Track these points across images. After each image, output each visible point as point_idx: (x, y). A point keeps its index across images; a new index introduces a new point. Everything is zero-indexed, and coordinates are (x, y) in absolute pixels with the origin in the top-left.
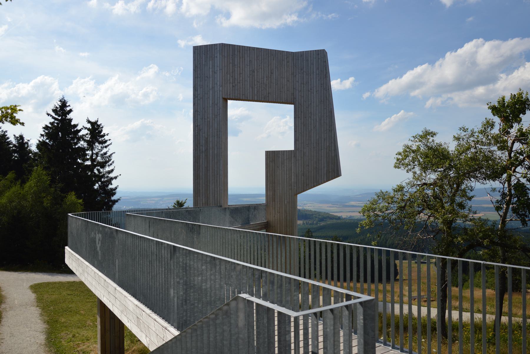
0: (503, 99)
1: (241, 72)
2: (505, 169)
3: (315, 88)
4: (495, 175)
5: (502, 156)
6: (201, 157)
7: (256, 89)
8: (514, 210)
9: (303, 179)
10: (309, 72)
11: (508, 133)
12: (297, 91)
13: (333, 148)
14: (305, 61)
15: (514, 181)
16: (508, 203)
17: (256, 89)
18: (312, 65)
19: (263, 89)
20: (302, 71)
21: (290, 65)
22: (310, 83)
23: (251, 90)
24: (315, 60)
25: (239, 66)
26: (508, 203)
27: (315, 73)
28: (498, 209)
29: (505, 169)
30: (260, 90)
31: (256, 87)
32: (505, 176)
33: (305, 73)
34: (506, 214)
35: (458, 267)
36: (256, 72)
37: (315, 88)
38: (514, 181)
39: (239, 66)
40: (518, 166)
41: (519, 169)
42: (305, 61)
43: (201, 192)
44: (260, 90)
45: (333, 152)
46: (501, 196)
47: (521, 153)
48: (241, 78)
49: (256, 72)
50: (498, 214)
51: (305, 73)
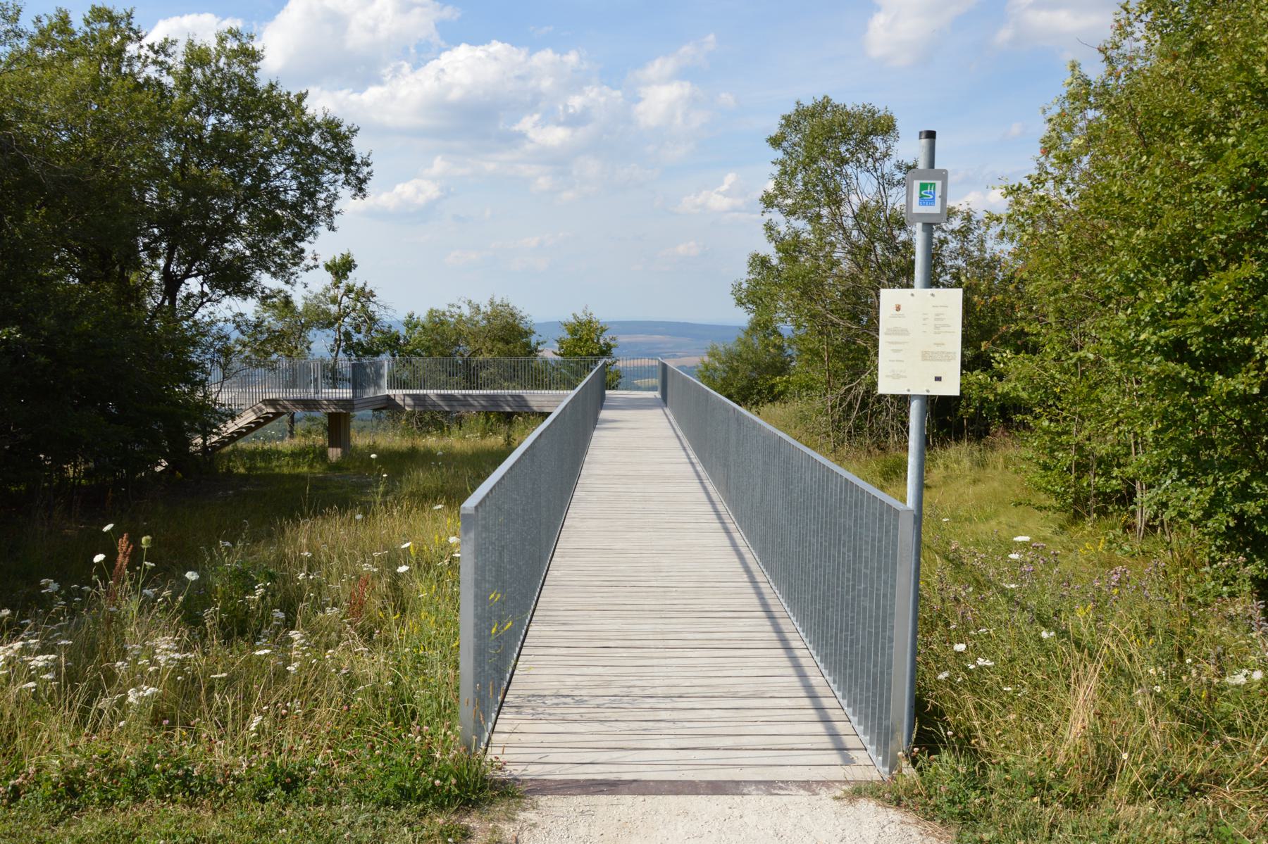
0: (360, 187)
2: (337, 319)
4: (330, 325)
5: (334, 309)
8: (344, 351)
11: (338, 287)
15: (343, 329)
16: (339, 346)
26: (339, 346)
28: (332, 351)
29: (337, 319)
32: (337, 325)
34: (337, 355)
35: (279, 454)
38: (343, 329)
40: (559, 124)
41: (346, 319)
46: (775, 142)
47: (348, 307)
50: (694, 475)
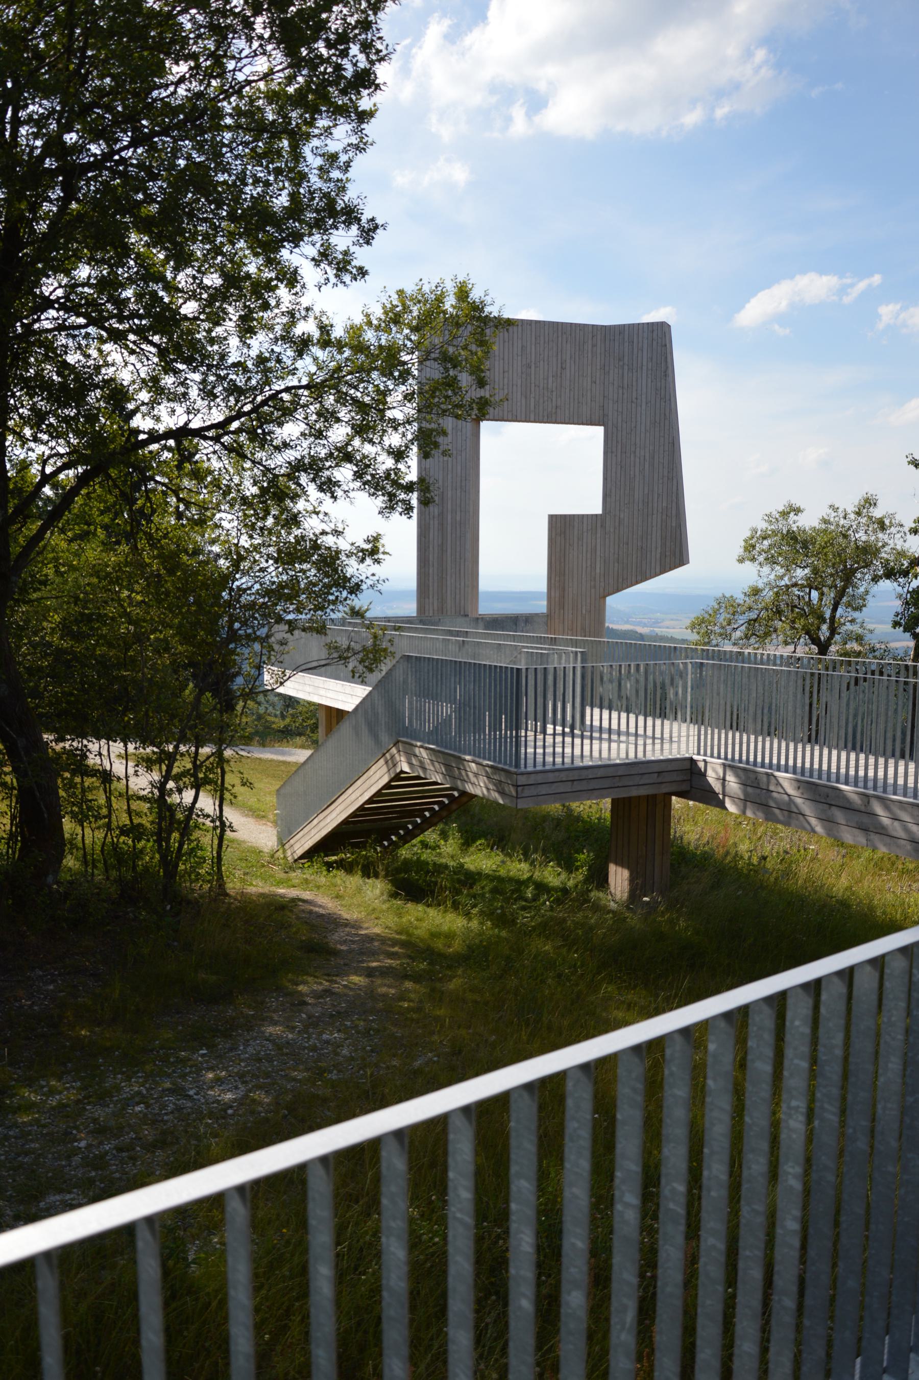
1: (506, 369)
3: (644, 396)
6: (432, 526)
7: (532, 400)
9: (616, 569)
10: (635, 365)
12: (611, 402)
13: (674, 512)
14: (626, 344)
17: (532, 400)
18: (640, 352)
19: (546, 398)
20: (621, 363)
21: (599, 352)
22: (634, 388)
23: (523, 401)
24: (645, 341)
25: (501, 356)
27: (645, 368)
30: (541, 401)
31: (533, 395)
33: (626, 367)
36: (533, 367)
37: (644, 396)
39: (501, 356)
42: (626, 344)
43: (431, 589)
44: (541, 401)
45: (674, 519)
48: (506, 380)
49: (533, 367)
51: (626, 367)
